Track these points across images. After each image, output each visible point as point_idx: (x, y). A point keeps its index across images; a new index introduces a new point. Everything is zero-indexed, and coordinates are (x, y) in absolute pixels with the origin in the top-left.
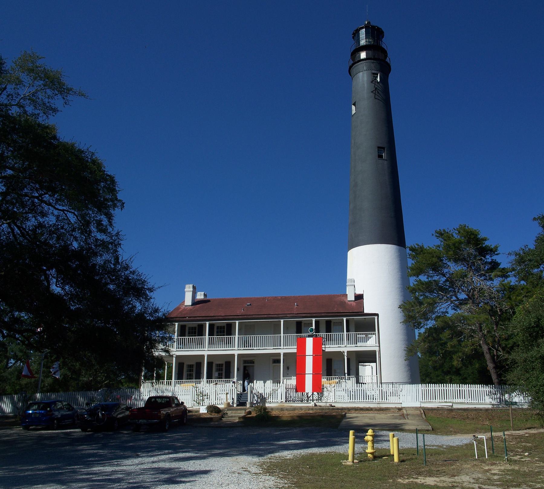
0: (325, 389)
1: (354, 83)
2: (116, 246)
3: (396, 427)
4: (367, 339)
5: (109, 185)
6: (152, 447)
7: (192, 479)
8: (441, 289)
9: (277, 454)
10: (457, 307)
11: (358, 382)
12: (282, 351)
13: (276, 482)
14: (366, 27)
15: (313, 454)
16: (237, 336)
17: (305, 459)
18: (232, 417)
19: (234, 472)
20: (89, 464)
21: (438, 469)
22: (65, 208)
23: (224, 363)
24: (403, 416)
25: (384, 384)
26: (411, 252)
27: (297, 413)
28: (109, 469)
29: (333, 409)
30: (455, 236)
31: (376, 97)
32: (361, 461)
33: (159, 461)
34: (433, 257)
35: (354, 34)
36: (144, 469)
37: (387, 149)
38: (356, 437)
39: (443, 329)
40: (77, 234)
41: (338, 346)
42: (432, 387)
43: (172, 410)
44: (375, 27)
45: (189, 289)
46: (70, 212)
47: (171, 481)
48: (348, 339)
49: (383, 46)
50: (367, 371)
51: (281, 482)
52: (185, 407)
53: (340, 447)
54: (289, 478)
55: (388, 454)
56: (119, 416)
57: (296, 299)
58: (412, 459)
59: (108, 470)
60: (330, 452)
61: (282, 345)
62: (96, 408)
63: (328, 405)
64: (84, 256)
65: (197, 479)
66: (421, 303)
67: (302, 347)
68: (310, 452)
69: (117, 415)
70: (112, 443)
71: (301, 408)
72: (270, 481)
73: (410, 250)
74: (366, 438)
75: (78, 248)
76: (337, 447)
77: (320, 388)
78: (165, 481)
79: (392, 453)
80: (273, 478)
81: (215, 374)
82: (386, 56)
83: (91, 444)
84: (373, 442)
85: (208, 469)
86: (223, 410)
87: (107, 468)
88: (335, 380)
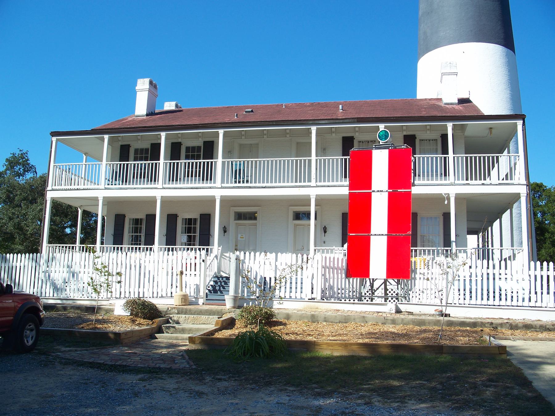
23: (198, 217)
45: (143, 84)
61: (313, 180)
81: (182, 237)
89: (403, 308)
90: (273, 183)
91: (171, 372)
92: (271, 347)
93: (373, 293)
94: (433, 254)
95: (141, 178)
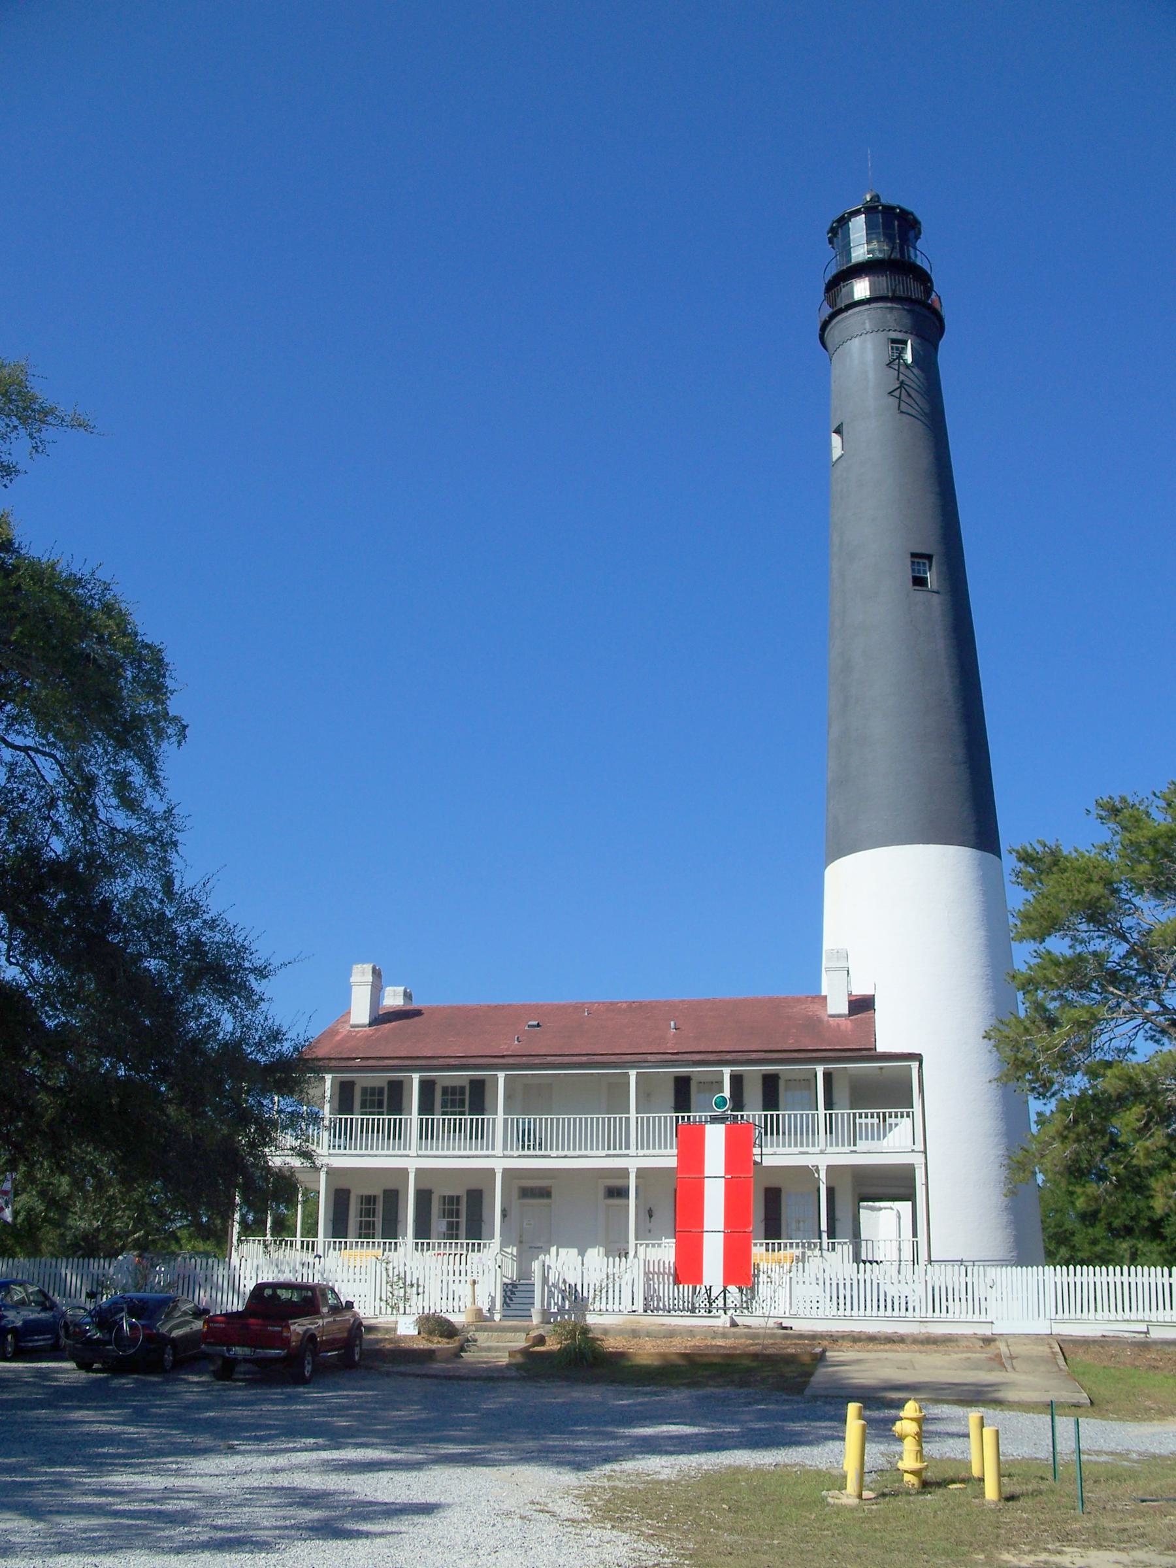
0: (763, 1278)
1: (836, 369)
2: (163, 846)
3: (979, 1393)
4: (883, 1129)
5: (147, 673)
6: (269, 1427)
7: (389, 1528)
8: (1114, 977)
9: (628, 1466)
10: (1163, 1032)
11: (857, 1258)
12: (633, 1161)
13: (634, 1550)
14: (869, 210)
15: (738, 1470)
16: (500, 1116)
17: (714, 1482)
18: (489, 1349)
19: (509, 1514)
20: (101, 1464)
21: (1121, 1525)
22: (30, 742)
24: (998, 1361)
25: (936, 1268)
26: (1022, 865)
27: (679, 1345)
28: (154, 1482)
29: (787, 1337)
30: (1157, 815)
31: (904, 407)
32: (884, 1495)
33: (292, 1468)
34: (1090, 880)
35: (833, 231)
36: (253, 1490)
37: (940, 560)
38: (870, 1423)
39: (1121, 1101)
40: (62, 814)
41: (800, 1149)
42: (1086, 1276)
43: (320, 1322)
44: (894, 208)
45: (361, 976)
46: (44, 754)
47: (329, 1530)
48: (830, 1130)
49: (920, 261)
50: (883, 1223)
51: (651, 1551)
52: (355, 1315)
53: (816, 1450)
54: (671, 1539)
55: (963, 1474)
56: (175, 1334)
57: (670, 1009)
58: (1041, 1493)
59: (153, 1486)
60: (786, 1465)
62: (114, 1308)
63: (771, 1323)
64: (78, 875)
65: (403, 1529)
66: (1052, 1023)
67: (691, 1148)
68: (726, 1462)
69: (170, 1331)
70: (160, 1406)
71: (691, 1332)
72: (619, 1545)
73: (1021, 859)
74: (898, 1427)
75: (64, 853)
76: (806, 1450)
77: (748, 1275)
78: (311, 1529)
79: (976, 1472)
80: (625, 1537)
81: (439, 1224)
82: (929, 291)
83: (105, 1408)
84: (921, 1437)
85: (432, 1499)
86: (464, 1329)
87: (150, 1478)
88: (789, 1251)
89: (739, 1320)
90: (576, 1150)
91: (505, 1379)
92: (595, 1358)
93: (711, 1304)
94: (803, 1247)
95: (373, 1132)
